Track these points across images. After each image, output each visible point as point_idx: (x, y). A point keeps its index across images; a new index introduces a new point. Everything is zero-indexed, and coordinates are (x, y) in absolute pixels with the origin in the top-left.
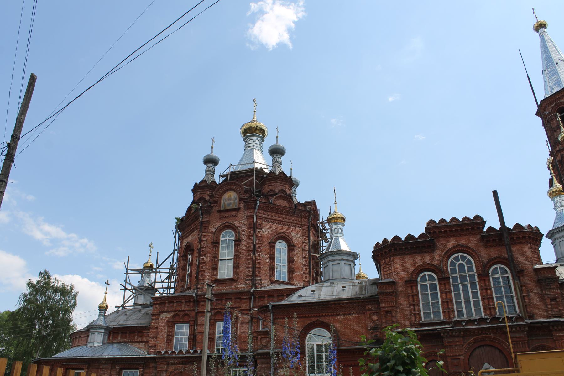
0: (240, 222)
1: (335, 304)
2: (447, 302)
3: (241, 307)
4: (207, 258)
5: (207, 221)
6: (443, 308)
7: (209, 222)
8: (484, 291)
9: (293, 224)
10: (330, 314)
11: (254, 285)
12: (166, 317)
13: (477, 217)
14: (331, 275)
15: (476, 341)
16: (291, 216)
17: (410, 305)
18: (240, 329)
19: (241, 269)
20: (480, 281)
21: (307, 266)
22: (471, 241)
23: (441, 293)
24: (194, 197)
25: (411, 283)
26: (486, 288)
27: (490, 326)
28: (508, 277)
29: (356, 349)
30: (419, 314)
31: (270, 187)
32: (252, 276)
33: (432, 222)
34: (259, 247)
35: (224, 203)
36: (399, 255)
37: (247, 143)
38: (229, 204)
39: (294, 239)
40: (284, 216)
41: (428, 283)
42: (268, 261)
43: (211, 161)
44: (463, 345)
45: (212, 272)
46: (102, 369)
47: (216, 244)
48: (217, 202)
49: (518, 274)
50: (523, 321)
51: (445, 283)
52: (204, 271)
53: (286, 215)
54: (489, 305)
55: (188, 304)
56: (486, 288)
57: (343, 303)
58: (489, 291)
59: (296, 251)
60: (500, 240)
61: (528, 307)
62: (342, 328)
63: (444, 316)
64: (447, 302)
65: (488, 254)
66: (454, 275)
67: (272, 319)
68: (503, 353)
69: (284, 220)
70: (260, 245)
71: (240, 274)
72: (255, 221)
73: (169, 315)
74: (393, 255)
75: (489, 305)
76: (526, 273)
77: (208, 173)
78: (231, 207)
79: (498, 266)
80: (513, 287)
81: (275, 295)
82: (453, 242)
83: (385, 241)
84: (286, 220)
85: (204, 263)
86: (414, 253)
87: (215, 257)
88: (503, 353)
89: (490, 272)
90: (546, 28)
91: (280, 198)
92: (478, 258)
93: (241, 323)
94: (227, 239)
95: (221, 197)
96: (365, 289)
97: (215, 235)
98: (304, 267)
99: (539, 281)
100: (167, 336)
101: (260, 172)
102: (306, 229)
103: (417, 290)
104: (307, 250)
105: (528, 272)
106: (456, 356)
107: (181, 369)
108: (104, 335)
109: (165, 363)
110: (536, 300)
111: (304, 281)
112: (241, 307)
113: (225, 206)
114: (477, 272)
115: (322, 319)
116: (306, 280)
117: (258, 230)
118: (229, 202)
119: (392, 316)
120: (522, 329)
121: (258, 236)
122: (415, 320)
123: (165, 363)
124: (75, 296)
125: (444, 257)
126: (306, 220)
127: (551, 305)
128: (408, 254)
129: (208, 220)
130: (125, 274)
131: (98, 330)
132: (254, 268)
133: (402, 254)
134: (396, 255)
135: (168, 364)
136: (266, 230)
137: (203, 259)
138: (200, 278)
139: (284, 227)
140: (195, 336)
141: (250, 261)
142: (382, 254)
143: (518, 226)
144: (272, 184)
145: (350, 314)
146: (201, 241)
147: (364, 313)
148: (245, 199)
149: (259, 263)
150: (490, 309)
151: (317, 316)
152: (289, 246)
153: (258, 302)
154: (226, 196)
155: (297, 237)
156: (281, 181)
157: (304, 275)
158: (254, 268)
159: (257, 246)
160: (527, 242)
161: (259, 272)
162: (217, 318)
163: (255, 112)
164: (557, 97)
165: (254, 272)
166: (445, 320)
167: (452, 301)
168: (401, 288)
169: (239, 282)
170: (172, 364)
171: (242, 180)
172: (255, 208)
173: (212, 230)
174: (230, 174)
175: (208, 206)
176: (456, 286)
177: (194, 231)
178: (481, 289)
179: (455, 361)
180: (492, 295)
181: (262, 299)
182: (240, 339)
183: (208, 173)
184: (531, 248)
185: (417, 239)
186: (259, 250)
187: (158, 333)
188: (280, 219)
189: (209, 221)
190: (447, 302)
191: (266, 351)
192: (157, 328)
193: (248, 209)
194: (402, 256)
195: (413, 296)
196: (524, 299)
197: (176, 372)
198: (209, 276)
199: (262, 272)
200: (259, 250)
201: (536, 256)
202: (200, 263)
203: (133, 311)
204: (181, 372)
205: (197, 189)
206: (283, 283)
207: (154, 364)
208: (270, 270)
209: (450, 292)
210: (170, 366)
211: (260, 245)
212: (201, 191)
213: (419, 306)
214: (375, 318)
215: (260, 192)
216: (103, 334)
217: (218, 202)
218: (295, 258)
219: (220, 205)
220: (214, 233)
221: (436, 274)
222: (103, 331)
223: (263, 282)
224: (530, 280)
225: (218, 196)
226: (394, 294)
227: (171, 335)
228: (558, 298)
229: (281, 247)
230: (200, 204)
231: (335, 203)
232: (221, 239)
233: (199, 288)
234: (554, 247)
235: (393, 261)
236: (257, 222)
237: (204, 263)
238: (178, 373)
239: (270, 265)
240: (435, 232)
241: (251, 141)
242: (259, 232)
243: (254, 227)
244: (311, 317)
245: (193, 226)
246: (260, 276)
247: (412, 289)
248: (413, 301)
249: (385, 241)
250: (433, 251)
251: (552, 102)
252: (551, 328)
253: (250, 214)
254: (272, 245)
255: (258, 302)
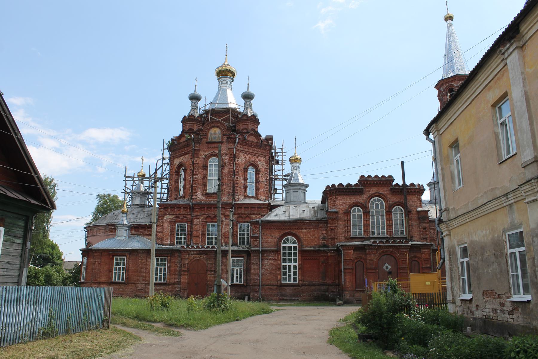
0: (224, 152)
1: (301, 222)
2: (367, 226)
3: (225, 214)
4: (199, 177)
5: (198, 149)
6: (364, 229)
7: (199, 150)
8: (388, 221)
9: (259, 155)
10: (297, 228)
11: (234, 199)
12: (169, 218)
13: (390, 176)
14: (292, 199)
15: (383, 252)
16: (258, 148)
17: (346, 226)
18: (224, 229)
19: (225, 187)
20: (386, 215)
21: (268, 185)
22: (384, 191)
23: (364, 220)
24: (183, 127)
25: (347, 213)
26: (389, 220)
27: (391, 245)
28: (402, 214)
29: (312, 250)
30: (350, 232)
31: (244, 126)
32: (232, 192)
33: (363, 176)
34: (237, 172)
35: (211, 137)
36: (341, 195)
37: (220, 83)
38: (215, 138)
39: (260, 166)
40: (253, 149)
41: (357, 213)
42: (243, 182)
43: (195, 98)
44: (376, 254)
45: (203, 188)
46: (140, 256)
47: (205, 167)
48: (205, 136)
49: (408, 213)
50: (408, 243)
51: (367, 215)
52: (197, 186)
53: (255, 148)
54: (390, 229)
55: (186, 210)
56: (389, 220)
57: (306, 222)
58: (391, 221)
59: (261, 175)
60: (401, 192)
61: (411, 233)
62: (304, 237)
63: (364, 234)
64: (367, 226)
65: (393, 199)
66: (372, 210)
67: (260, 229)
68: (396, 259)
69: (254, 152)
70: (238, 170)
71: (223, 190)
72: (235, 153)
73: (171, 217)
74: (338, 195)
75: (390, 229)
76: (413, 213)
77: (193, 108)
78: (216, 140)
79: (398, 207)
80: (404, 226)
81: (250, 207)
82: (374, 190)
83: (333, 185)
84: (255, 152)
85: (197, 180)
86: (350, 195)
87: (205, 177)
88: (396, 259)
89: (393, 210)
90: (452, 20)
91: (251, 135)
92: (388, 201)
93: (225, 225)
94: (214, 164)
95: (208, 131)
96: (317, 213)
97: (205, 160)
98: (266, 186)
99: (419, 218)
100: (171, 231)
101: (234, 110)
102: (268, 158)
103: (350, 217)
104: (268, 174)
105: (414, 212)
106: (372, 259)
107: (198, 258)
108: (128, 231)
109: (187, 254)
110: (415, 228)
111: (266, 196)
112: (225, 214)
113: (212, 138)
114: (385, 209)
115: (292, 231)
116: (267, 195)
117: (236, 159)
118: (215, 136)
119: (335, 232)
120: (407, 247)
121: (237, 163)
122: (348, 235)
123: (187, 254)
124: (54, 186)
125: (368, 199)
126: (268, 152)
127: (423, 231)
128: (347, 195)
129: (199, 148)
130: (124, 180)
131: (124, 228)
132: (234, 187)
133: (343, 195)
134: (340, 195)
135: (189, 254)
136: (242, 159)
137: (196, 178)
138: (194, 191)
139: (253, 157)
140: (192, 232)
141: (231, 181)
142: (330, 193)
143: (412, 184)
144: (246, 124)
145: (309, 229)
146: (193, 164)
147: (317, 229)
148: (227, 135)
149: (237, 183)
150: (390, 231)
151: (288, 229)
152: (256, 171)
153: (237, 211)
154: (212, 131)
155: (262, 165)
156: (252, 122)
157: (266, 192)
158: (234, 187)
159: (236, 171)
160: (416, 194)
161: (237, 190)
162: (207, 220)
163: (226, 55)
164: (450, 80)
165: (234, 190)
166: (364, 236)
167: (369, 226)
168: (341, 216)
169: (223, 196)
170: (192, 255)
171: (219, 115)
172: (235, 143)
173: (202, 156)
174: (211, 110)
175: (198, 138)
176: (373, 216)
177: (186, 154)
178: (387, 220)
179: (371, 262)
180: (392, 224)
181: (240, 209)
182: (224, 236)
183: (193, 108)
184: (418, 198)
185: (353, 186)
186: (238, 174)
187: (163, 229)
188: (251, 151)
189: (200, 149)
190: (367, 226)
191: (257, 249)
192: (162, 226)
193: (229, 143)
194: (343, 196)
195: (347, 221)
196: (409, 227)
197: (194, 259)
198: (200, 190)
199: (239, 189)
200: (238, 174)
201: (420, 202)
202: (193, 181)
203: (137, 211)
204: (198, 259)
205: (185, 121)
206: (252, 197)
207: (178, 254)
208: (244, 188)
209: (369, 220)
210: (190, 256)
211: (238, 170)
212: (190, 123)
213: (351, 227)
214: (324, 232)
215: (235, 127)
216: (127, 230)
217: (206, 135)
218: (260, 180)
219: (208, 138)
220: (204, 159)
221: (362, 208)
222: (128, 228)
223: (239, 196)
224: (414, 216)
225: (206, 131)
226: (337, 219)
227: (174, 231)
228: (427, 228)
229: (251, 171)
230: (192, 135)
231: (226, 55)
232: (209, 164)
233: (194, 198)
234: (430, 192)
235: (337, 198)
236: (236, 153)
237: (197, 180)
238: (196, 260)
239: (244, 184)
240: (364, 183)
241: (225, 82)
242: (238, 161)
243: (234, 157)
244: (285, 229)
245: (185, 150)
246: (237, 193)
247: (347, 217)
248: (347, 224)
249: (333, 185)
250: (361, 195)
251: (447, 83)
252: (421, 247)
253: (231, 147)
254: (246, 170)
255: (237, 211)
